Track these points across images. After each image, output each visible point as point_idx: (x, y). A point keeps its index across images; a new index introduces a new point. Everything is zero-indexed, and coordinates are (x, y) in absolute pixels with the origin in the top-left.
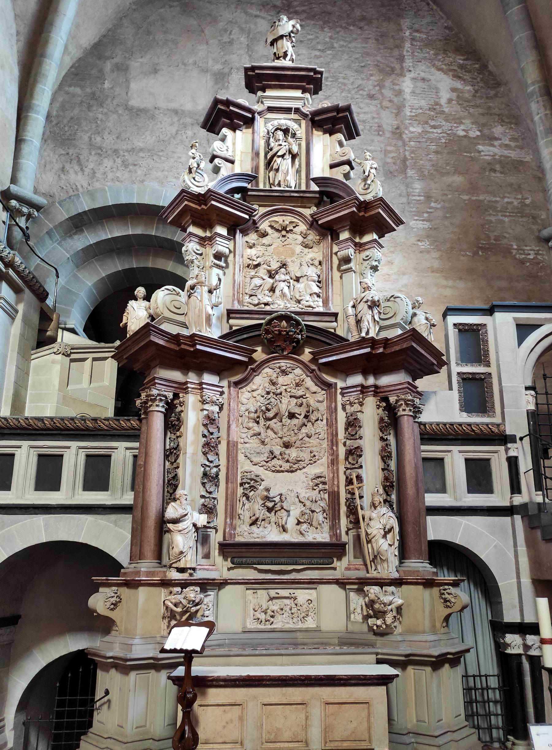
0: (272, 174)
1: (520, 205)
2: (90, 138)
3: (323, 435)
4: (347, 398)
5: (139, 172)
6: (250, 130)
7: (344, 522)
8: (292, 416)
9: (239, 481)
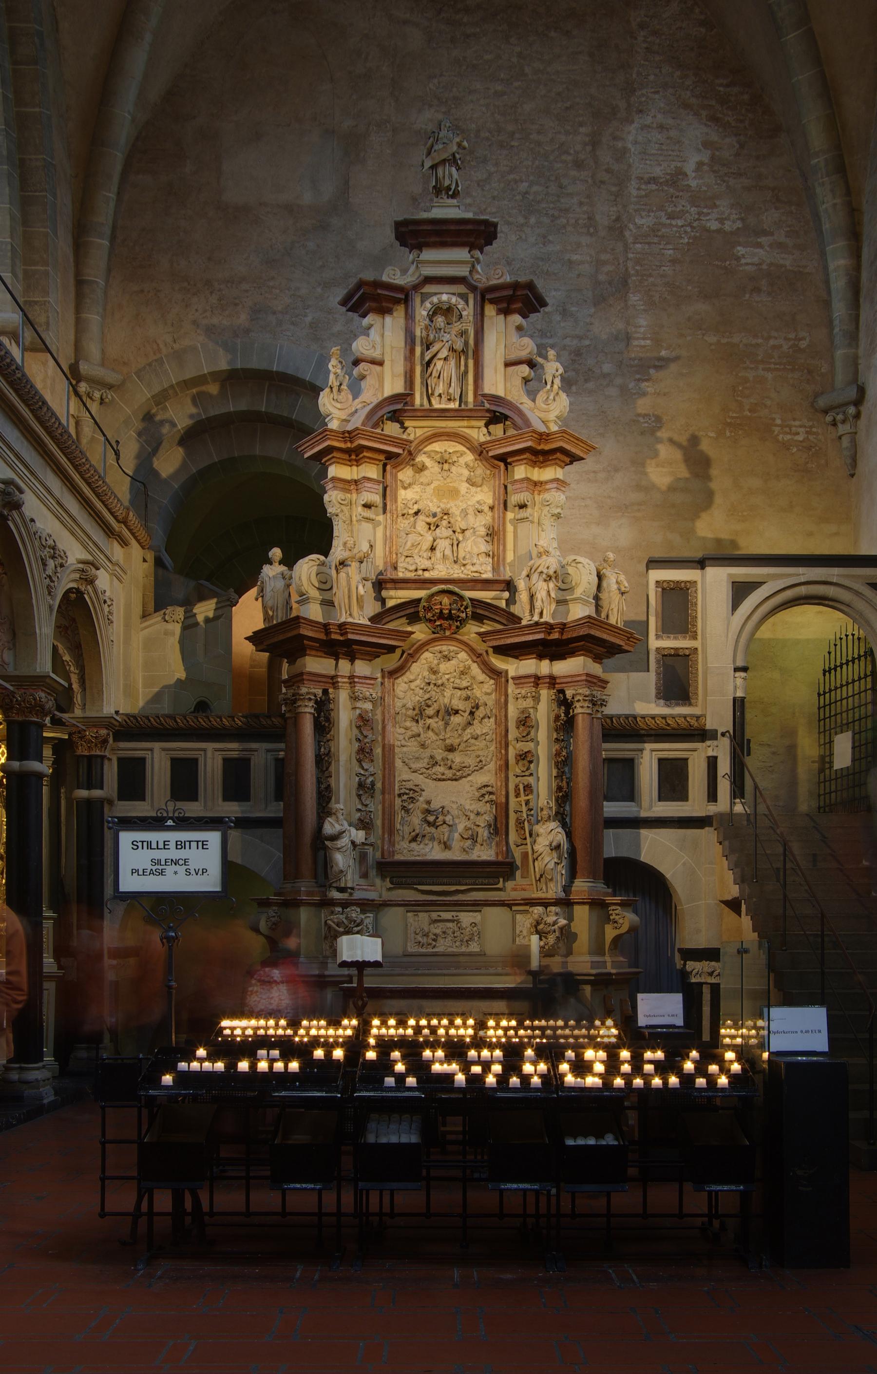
1: (791, 350)
4: (518, 691)
9: (397, 792)
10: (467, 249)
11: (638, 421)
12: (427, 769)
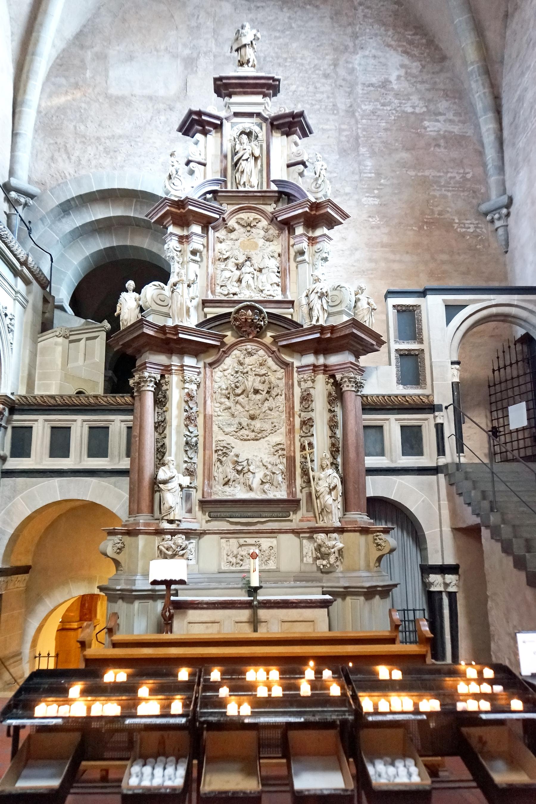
0: (238, 175)
1: (461, 180)
2: (75, 127)
4: (301, 376)
5: (119, 158)
6: (219, 134)
7: (299, 481)
8: (256, 392)
9: (214, 448)
11: (369, 221)
12: (236, 432)
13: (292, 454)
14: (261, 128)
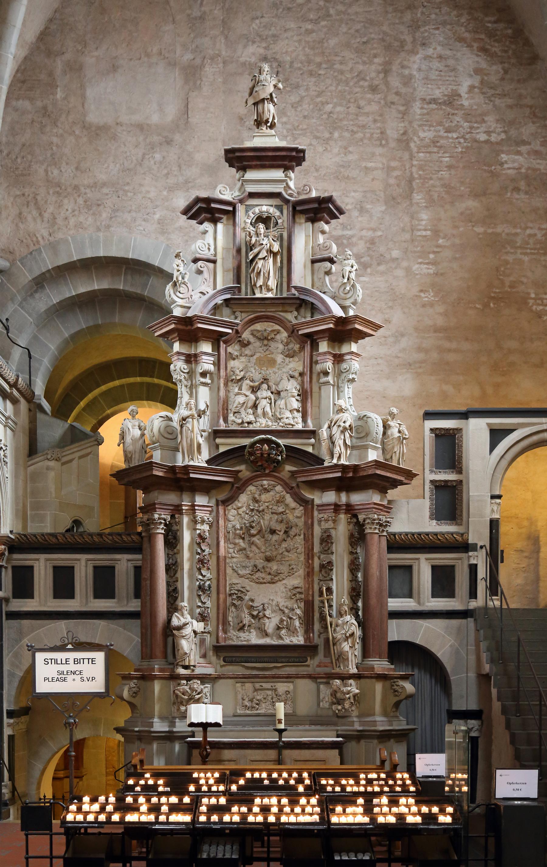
1: (543, 238)
3: (301, 549)
5: (104, 215)
8: (273, 532)
10: (282, 170)
11: (420, 296)
13: (311, 598)
14: (282, 212)
